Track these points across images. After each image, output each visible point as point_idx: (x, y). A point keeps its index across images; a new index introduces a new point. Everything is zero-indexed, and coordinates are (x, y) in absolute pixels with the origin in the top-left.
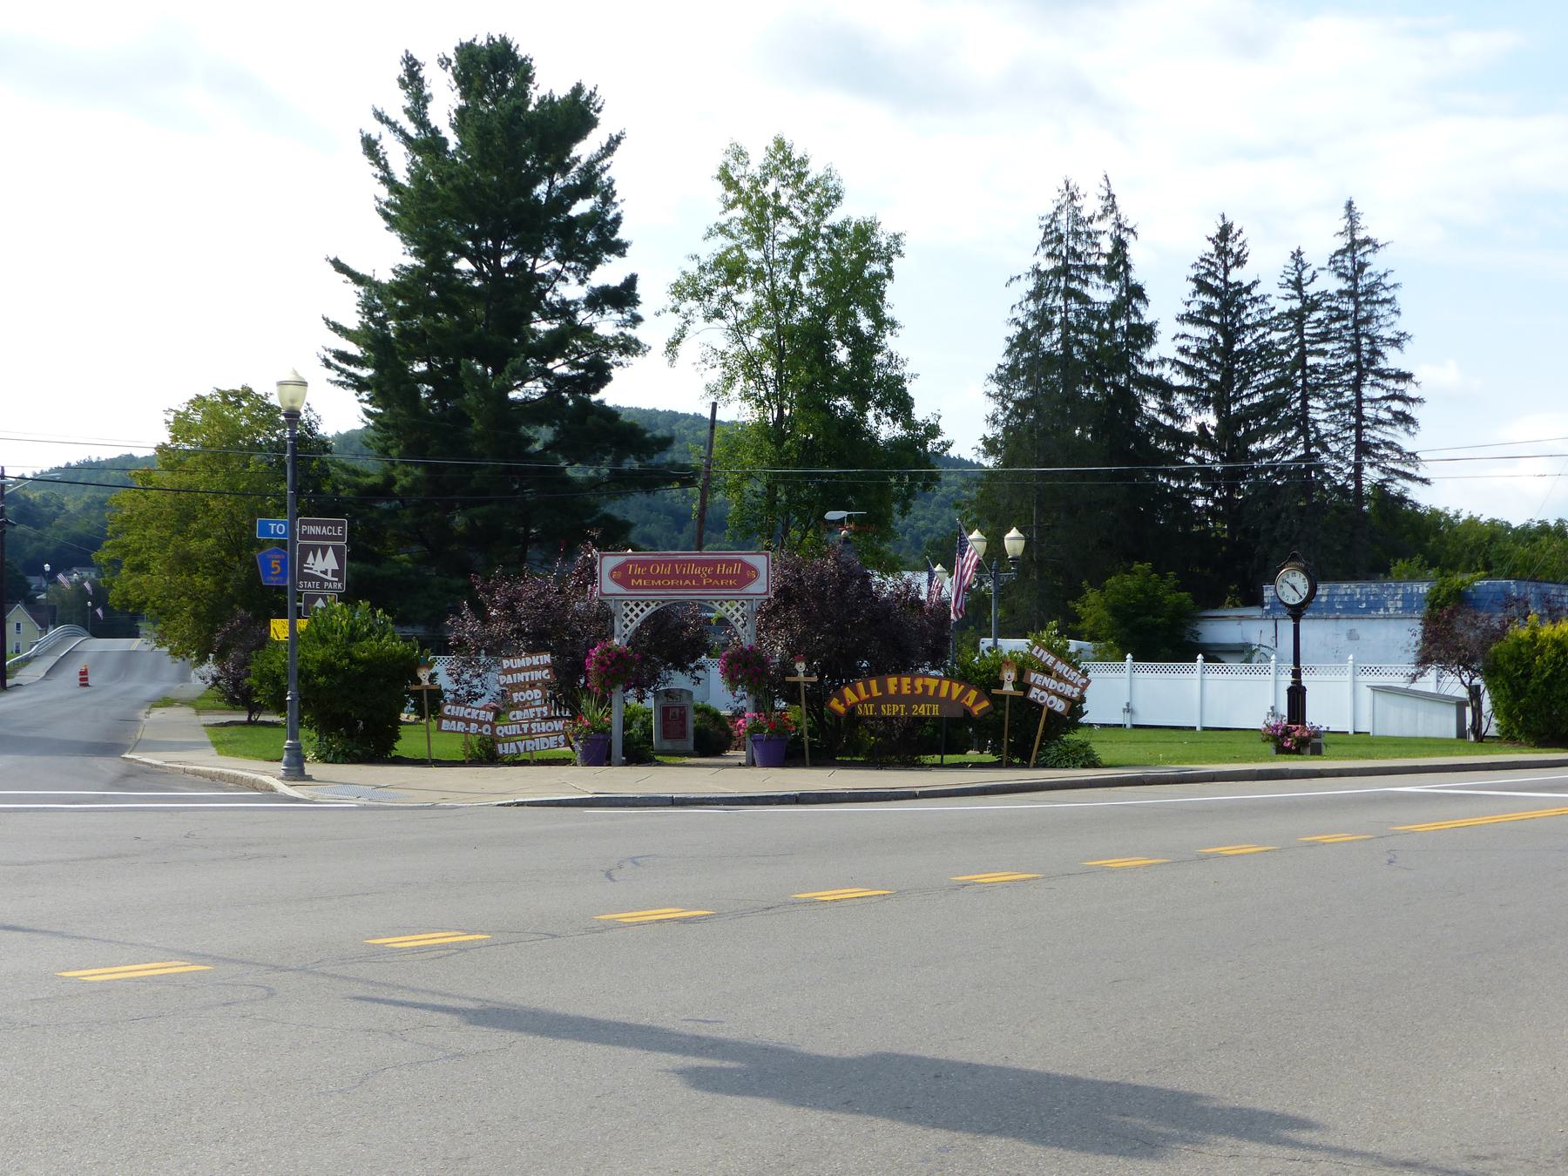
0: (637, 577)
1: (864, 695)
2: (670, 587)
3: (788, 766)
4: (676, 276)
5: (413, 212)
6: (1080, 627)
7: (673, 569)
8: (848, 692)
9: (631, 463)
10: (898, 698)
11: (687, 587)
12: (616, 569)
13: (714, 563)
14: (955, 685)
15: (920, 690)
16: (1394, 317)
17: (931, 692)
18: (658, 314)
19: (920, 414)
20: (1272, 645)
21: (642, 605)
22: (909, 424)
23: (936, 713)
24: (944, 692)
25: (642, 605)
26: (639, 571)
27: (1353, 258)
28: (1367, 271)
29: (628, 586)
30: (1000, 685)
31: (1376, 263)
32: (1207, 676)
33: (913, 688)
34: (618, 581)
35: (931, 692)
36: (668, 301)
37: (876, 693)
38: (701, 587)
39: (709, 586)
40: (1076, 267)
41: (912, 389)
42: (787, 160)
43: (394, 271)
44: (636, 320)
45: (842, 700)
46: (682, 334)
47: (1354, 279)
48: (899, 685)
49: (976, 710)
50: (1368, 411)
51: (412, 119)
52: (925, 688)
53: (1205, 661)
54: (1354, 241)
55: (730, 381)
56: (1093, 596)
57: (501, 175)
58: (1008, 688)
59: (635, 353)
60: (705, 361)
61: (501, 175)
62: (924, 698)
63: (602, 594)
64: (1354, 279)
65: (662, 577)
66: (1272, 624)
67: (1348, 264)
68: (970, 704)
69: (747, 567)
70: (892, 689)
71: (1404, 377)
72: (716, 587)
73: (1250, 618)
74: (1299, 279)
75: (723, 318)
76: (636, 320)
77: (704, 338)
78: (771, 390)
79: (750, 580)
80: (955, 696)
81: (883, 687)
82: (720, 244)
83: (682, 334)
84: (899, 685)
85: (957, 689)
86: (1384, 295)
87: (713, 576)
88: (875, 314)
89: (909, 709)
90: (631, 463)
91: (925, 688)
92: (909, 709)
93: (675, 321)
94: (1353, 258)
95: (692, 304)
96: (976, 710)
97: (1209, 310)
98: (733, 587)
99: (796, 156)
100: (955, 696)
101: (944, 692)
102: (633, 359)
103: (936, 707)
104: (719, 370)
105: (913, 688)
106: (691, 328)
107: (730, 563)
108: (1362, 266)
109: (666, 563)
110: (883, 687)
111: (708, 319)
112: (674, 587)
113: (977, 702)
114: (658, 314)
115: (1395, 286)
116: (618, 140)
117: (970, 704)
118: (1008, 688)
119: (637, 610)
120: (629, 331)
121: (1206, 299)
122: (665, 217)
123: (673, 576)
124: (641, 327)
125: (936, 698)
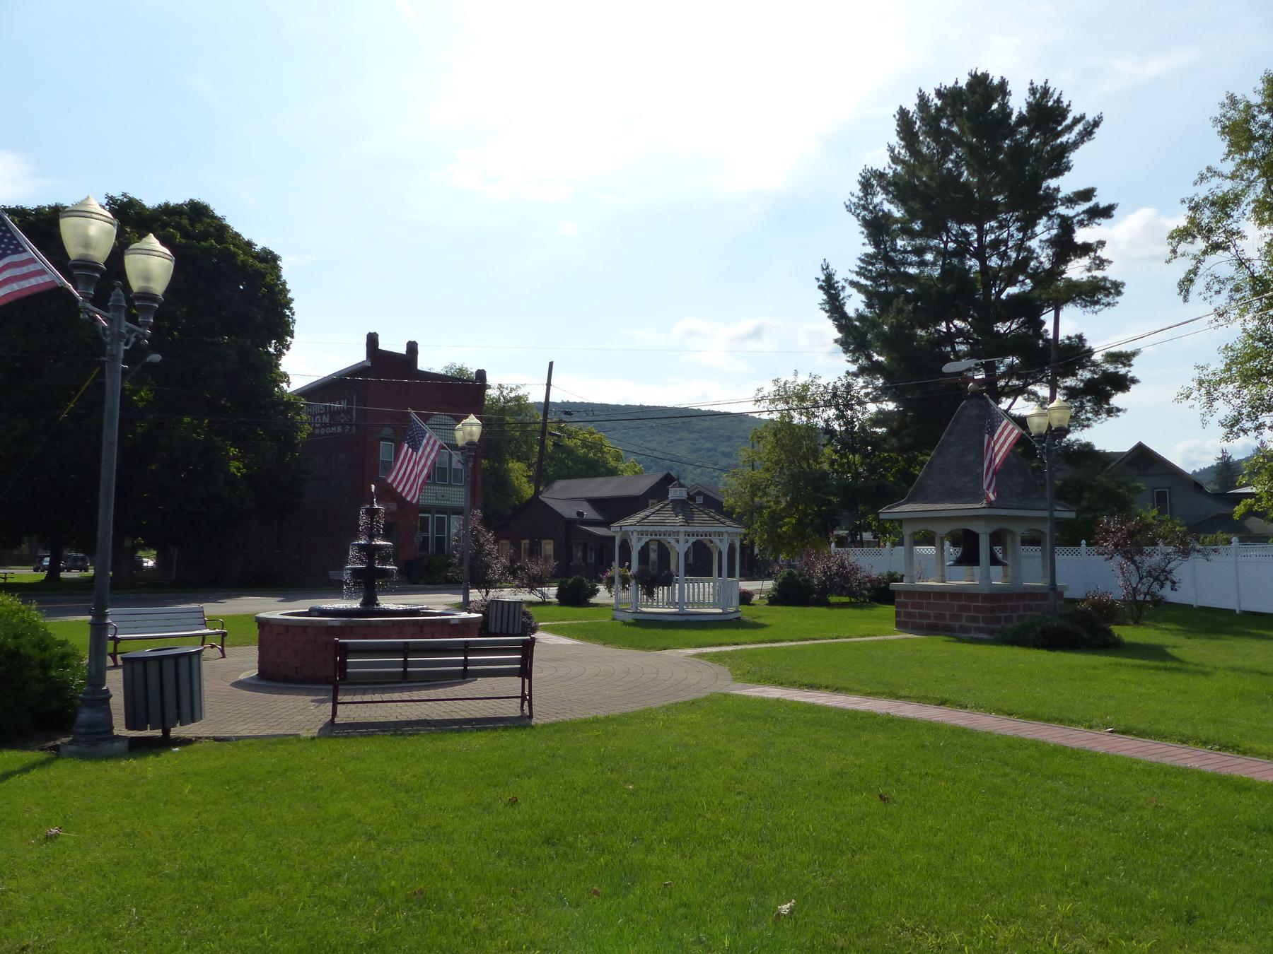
44: (1101, 263)
46: (1194, 271)
59: (1119, 293)
76: (1101, 263)
116: (1096, 124)
120: (1099, 274)
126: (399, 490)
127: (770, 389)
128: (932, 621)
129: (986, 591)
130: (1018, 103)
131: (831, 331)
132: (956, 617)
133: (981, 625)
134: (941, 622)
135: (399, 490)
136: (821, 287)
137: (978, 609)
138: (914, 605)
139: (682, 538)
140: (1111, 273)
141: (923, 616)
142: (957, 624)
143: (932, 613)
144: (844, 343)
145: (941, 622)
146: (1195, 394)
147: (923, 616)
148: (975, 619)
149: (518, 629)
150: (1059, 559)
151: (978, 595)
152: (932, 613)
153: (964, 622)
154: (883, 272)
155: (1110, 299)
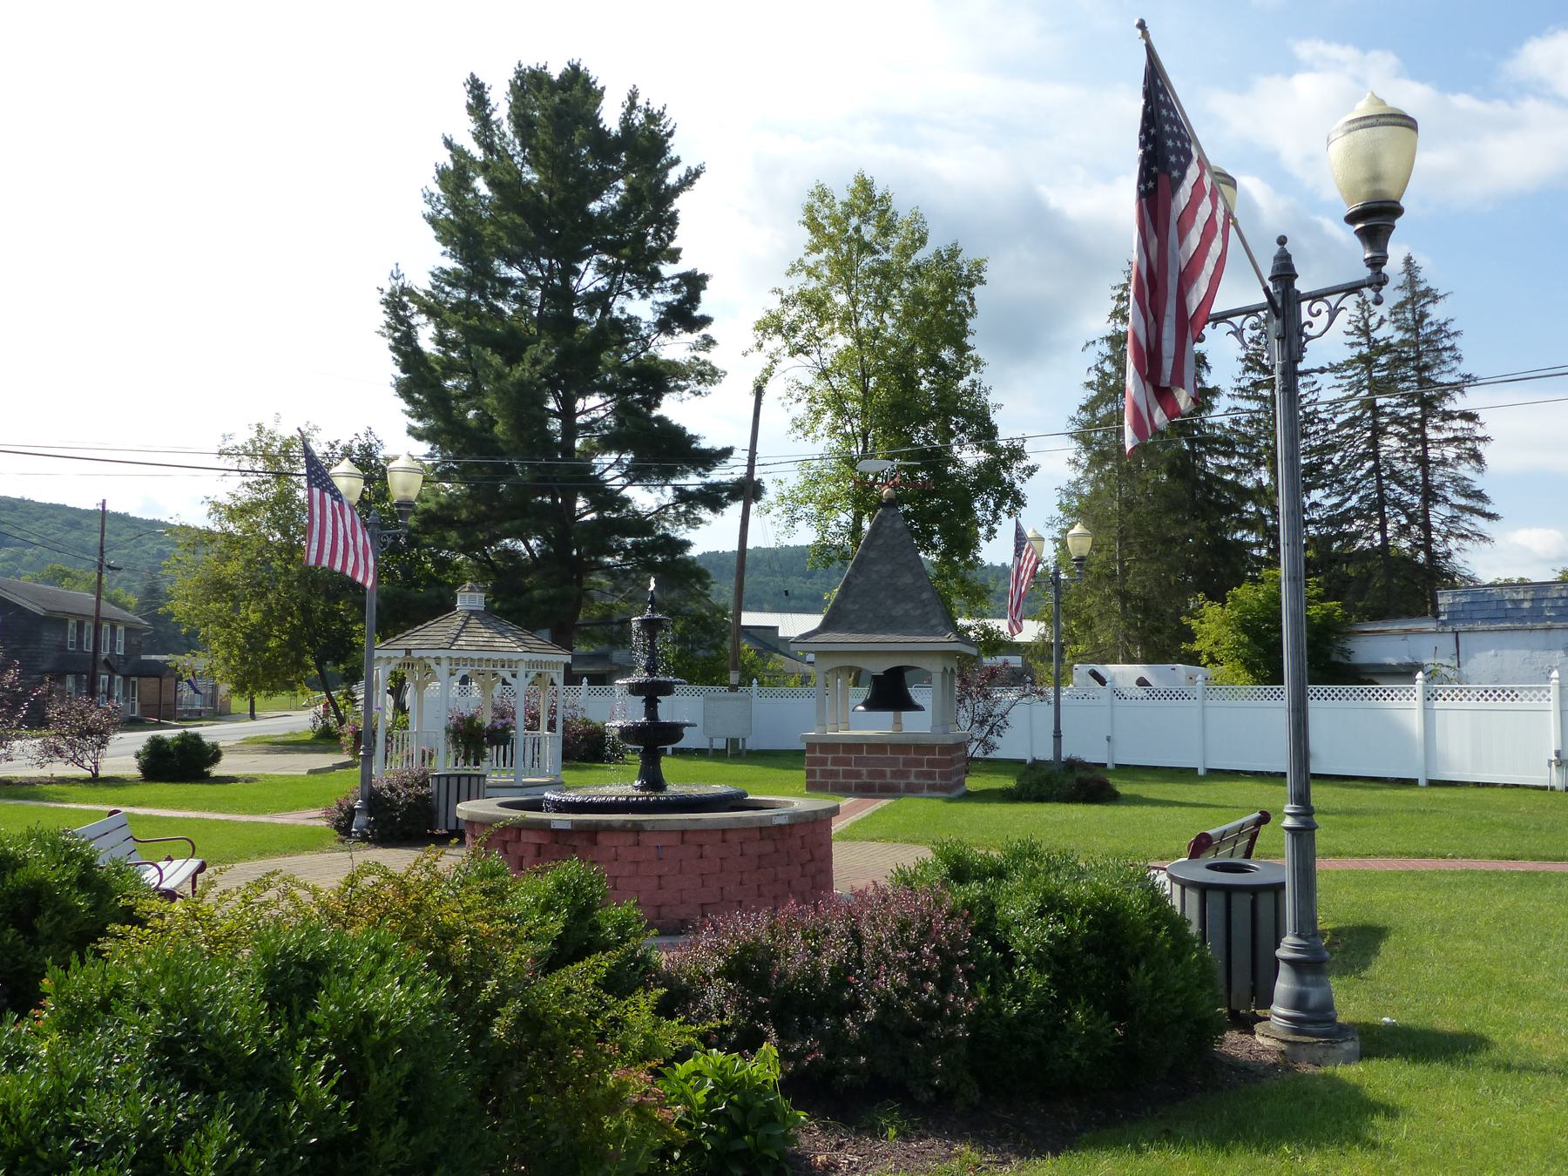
4: (761, 315)
5: (461, 230)
6: (1197, 647)
9: (692, 481)
16: (1455, 363)
18: (745, 354)
19: (1004, 437)
20: (1454, 664)
22: (992, 448)
27: (1414, 310)
28: (1427, 321)
31: (1436, 313)
32: (1439, 704)
36: (751, 339)
41: (995, 418)
42: (870, 199)
43: (433, 275)
44: (709, 342)
46: (769, 372)
47: (1415, 331)
50: (1433, 454)
51: (481, 144)
53: (589, 683)
54: (1414, 294)
55: (818, 415)
56: (1212, 610)
57: (564, 191)
59: (712, 382)
60: (790, 395)
61: (564, 191)
64: (1415, 331)
66: (1451, 639)
67: (1409, 315)
71: (1469, 417)
73: (1420, 632)
74: (1366, 324)
75: (807, 354)
76: (709, 342)
77: (791, 374)
78: (857, 430)
82: (800, 282)
83: (769, 372)
86: (1447, 343)
88: (962, 349)
90: (692, 481)
93: (760, 361)
94: (1414, 310)
95: (778, 341)
97: (1256, 385)
99: (878, 194)
102: (712, 388)
104: (804, 404)
106: (778, 368)
108: (1423, 316)
111: (792, 354)
114: (745, 354)
115: (1456, 334)
116: (697, 174)
120: (702, 355)
121: (1255, 376)
122: (736, 240)
124: (714, 350)
126: (338, 567)
127: (244, 436)
128: (865, 779)
129: (895, 740)
130: (610, 117)
131: (389, 370)
132: (903, 774)
133: (938, 781)
134: (878, 781)
135: (338, 567)
136: (386, 303)
137: (931, 763)
138: (836, 762)
139: (522, 669)
140: (714, 357)
141: (848, 774)
142: (902, 783)
143: (864, 770)
144: (405, 390)
145: (878, 781)
146: (777, 510)
147: (848, 774)
148: (930, 775)
149: (529, 838)
150: (1312, 704)
151: (861, 745)
152: (864, 770)
153: (912, 780)
154: (467, 305)
155: (701, 388)
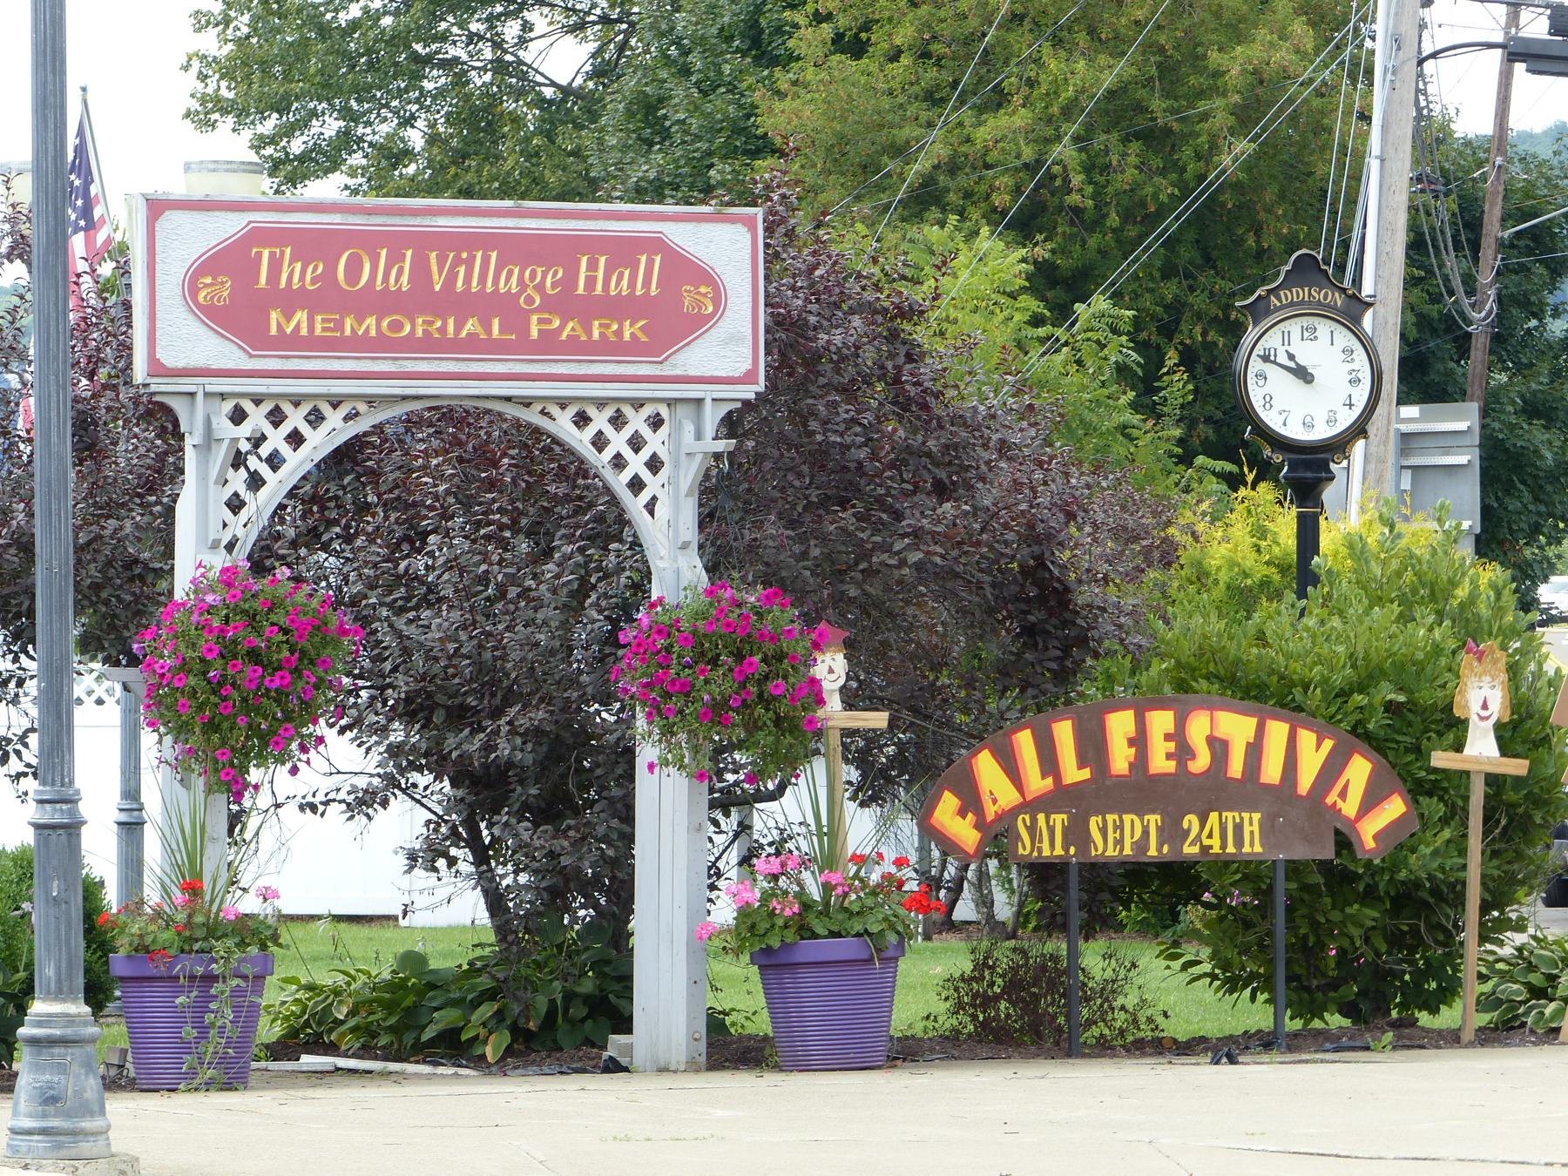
0: (290, 301)
1: (1037, 783)
2: (413, 345)
3: (123, 773)
7: (421, 271)
8: (986, 767)
10: (1141, 791)
11: (472, 345)
12: (212, 265)
13: (564, 251)
14: (1307, 738)
15: (1202, 761)
17: (1236, 768)
21: (296, 419)
23: (1253, 847)
24: (1272, 771)
25: (296, 419)
26: (295, 274)
29: (251, 333)
30: (1453, 728)
33: (1183, 752)
34: (218, 317)
35: (1236, 768)
37: (1073, 773)
38: (522, 346)
39: (549, 344)
40: (439, 577)
45: (971, 802)
48: (1139, 741)
49: (1369, 831)
52: (1219, 747)
58: (1481, 748)
62: (1216, 791)
63: (157, 369)
65: (385, 302)
68: (1350, 808)
69: (685, 270)
70: (1121, 758)
72: (575, 347)
79: (695, 324)
80: (1306, 779)
81: (1093, 747)
84: (1139, 741)
85: (1313, 754)
87: (563, 303)
89: (1077, 833)
91: (1219, 747)
92: (1077, 833)
96: (1369, 831)
98: (633, 349)
100: (1306, 779)
101: (1272, 771)
103: (1252, 822)
105: (1183, 752)
107: (623, 252)
109: (396, 243)
110: (1093, 747)
112: (428, 345)
113: (1371, 801)
117: (1350, 808)
118: (1481, 748)
119: (276, 440)
123: (421, 299)
125: (1248, 791)
